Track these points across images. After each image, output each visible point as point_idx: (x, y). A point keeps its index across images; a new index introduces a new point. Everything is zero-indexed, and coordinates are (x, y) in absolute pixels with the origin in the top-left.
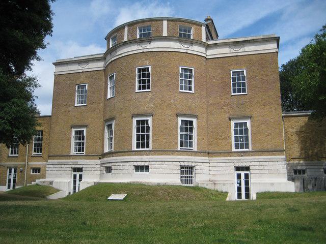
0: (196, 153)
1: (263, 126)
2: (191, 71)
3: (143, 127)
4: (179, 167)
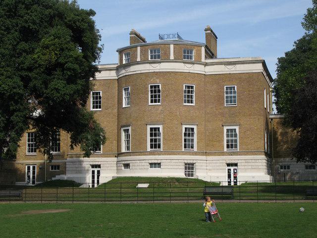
0: (196, 154)
1: (248, 132)
2: (192, 87)
3: (155, 132)
4: (184, 164)
